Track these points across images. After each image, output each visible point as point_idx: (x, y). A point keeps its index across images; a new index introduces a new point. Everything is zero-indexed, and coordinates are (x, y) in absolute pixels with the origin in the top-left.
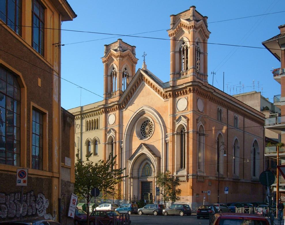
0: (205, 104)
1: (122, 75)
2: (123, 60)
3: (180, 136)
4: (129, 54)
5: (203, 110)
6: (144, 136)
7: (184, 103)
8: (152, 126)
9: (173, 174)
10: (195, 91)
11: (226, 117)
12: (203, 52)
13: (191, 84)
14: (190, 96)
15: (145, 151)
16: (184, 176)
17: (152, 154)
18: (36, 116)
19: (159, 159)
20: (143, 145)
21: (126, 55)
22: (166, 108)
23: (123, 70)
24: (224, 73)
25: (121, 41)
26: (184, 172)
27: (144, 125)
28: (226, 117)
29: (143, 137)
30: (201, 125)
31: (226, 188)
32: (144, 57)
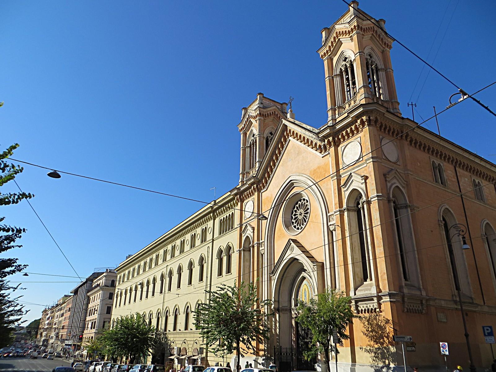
0: (401, 150)
1: (265, 141)
2: (266, 121)
3: (356, 213)
4: (275, 112)
5: (398, 160)
6: (297, 227)
7: (356, 149)
8: (306, 204)
9: (348, 294)
10: (372, 123)
11: (455, 180)
12: (383, 67)
13: (362, 109)
14: (365, 134)
15: (296, 253)
16: (370, 299)
17: (307, 257)
18: (469, 349)
19: (321, 266)
20: (291, 242)
21: (270, 113)
22: (327, 165)
23: (267, 134)
24: (434, 107)
25: (262, 96)
26: (369, 288)
27: (295, 209)
28: (453, 180)
29: (296, 229)
30: (397, 187)
31: (485, 328)
32: (290, 103)
